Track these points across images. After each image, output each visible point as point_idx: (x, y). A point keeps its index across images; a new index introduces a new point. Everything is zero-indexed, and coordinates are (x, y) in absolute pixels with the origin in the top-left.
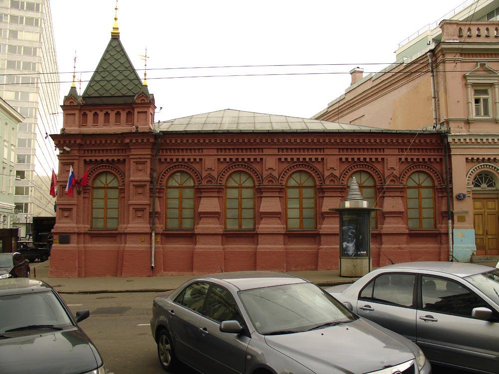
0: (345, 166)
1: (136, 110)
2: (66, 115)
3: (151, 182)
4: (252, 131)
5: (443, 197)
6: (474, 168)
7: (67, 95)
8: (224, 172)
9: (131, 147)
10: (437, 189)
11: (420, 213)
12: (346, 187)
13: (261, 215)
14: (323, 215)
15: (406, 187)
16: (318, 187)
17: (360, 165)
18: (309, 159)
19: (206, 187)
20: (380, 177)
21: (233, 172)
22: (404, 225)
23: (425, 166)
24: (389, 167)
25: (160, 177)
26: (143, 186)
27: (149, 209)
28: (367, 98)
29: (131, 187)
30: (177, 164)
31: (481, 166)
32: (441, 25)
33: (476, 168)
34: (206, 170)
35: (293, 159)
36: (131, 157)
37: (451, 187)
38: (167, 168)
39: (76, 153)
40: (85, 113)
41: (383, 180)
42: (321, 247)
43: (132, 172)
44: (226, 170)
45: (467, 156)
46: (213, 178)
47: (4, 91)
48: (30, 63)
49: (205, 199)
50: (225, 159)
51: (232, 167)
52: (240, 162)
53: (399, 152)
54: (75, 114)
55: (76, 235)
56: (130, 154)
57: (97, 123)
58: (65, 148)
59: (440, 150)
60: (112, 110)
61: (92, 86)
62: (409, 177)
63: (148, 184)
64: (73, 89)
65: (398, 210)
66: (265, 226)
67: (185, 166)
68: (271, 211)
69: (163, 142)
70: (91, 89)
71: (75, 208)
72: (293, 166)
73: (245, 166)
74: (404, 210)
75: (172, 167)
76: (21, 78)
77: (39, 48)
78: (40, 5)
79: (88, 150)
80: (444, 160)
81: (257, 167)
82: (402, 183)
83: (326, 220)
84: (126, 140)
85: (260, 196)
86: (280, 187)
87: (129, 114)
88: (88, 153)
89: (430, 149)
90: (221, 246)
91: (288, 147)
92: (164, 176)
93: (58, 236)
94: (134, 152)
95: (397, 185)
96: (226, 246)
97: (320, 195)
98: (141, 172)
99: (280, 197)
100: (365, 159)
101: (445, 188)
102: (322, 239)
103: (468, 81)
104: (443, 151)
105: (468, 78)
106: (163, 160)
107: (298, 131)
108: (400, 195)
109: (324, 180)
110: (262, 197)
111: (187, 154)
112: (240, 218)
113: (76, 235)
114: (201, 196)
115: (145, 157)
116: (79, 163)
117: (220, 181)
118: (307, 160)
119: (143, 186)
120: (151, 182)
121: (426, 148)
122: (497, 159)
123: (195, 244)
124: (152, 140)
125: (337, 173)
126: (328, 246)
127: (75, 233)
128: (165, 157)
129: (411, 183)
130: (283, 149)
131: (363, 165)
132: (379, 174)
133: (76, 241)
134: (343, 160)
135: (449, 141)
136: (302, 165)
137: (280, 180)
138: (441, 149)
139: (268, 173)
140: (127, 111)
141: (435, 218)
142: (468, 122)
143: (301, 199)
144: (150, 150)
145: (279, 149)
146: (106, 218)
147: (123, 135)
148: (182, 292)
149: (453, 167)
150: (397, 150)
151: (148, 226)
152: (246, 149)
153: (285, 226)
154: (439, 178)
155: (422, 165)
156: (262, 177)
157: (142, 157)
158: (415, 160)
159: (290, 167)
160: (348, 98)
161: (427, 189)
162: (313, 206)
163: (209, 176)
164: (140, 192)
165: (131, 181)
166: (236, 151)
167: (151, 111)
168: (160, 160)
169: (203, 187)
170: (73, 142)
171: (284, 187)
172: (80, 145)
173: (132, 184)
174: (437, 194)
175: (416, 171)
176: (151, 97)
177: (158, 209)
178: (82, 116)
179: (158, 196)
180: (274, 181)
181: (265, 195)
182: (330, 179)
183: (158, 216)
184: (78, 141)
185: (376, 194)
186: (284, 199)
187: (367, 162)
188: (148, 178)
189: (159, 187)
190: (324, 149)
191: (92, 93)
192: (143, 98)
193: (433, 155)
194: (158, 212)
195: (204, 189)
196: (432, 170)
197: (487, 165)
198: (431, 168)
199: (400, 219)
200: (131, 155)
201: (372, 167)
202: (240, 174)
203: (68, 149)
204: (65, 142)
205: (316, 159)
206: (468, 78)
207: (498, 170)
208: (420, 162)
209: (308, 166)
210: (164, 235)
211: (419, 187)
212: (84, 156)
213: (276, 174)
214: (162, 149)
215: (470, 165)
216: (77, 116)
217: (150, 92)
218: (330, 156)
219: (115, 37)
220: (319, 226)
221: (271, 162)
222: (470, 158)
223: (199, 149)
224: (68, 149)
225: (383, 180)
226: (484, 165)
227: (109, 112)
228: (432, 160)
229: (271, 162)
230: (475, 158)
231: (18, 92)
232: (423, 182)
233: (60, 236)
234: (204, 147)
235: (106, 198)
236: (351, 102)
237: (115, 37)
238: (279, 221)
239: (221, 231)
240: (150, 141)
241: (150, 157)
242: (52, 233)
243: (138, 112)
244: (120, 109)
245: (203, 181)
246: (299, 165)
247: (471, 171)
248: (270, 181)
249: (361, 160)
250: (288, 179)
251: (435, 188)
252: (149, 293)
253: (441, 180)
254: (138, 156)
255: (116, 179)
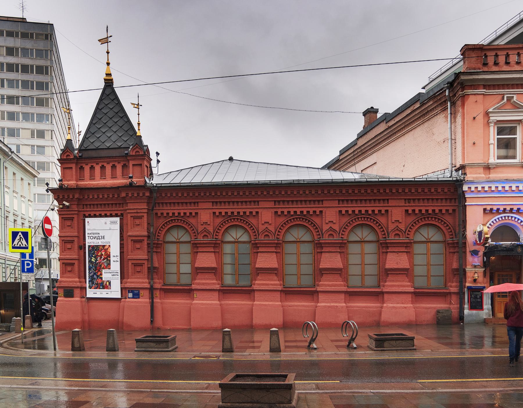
0: (345, 220)
1: (131, 163)
2: (64, 169)
3: (149, 237)
4: (401, 180)
5: (454, 252)
6: (490, 222)
7: (151, 162)
8: (220, 226)
9: (127, 202)
10: (448, 243)
11: (428, 271)
12: (346, 242)
13: (257, 271)
14: (321, 272)
15: (412, 241)
16: (316, 242)
17: (361, 218)
18: (281, 212)
19: (202, 242)
20: (383, 231)
21: (229, 227)
22: (409, 283)
23: (435, 218)
24: (394, 219)
25: (157, 232)
26: (141, 241)
27: (148, 264)
28: (406, 126)
29: (129, 240)
30: (173, 218)
31: (502, 217)
32: (462, 52)
33: (495, 220)
34: (263, 224)
35: (341, 211)
36: (128, 211)
37: (463, 241)
38: (163, 223)
39: (75, 208)
40: (82, 167)
41: (386, 234)
42: (319, 304)
43: (129, 228)
44: (222, 224)
45: (485, 207)
46: (209, 232)
47: (496, 252)
48: (28, 81)
49: (262, 254)
50: (220, 213)
51: (228, 221)
52: (236, 216)
53: (405, 203)
54: (72, 168)
55: (158, 291)
56: (127, 208)
57: (105, 177)
58: (64, 202)
59: (453, 201)
60: (107, 163)
61: (87, 138)
62: (417, 230)
63: (146, 239)
64: (69, 142)
65: (402, 267)
66: (260, 283)
67: (181, 220)
68: (268, 267)
69: (158, 195)
70: (509, 282)
71: (76, 219)
72: (290, 220)
73: (241, 220)
74: (409, 267)
75: (169, 221)
76: (35, 98)
77: (51, 83)
78: (49, 67)
79: (86, 205)
80: (457, 211)
81: (253, 221)
82: (407, 237)
83: (390, 277)
84: (122, 195)
85: (385, 251)
86: (276, 242)
87: (125, 167)
88: (87, 208)
89: (442, 199)
90: (218, 302)
91: (285, 199)
92: (346, 229)
93: (63, 290)
94: (130, 206)
95: (402, 239)
96: (223, 302)
97: (318, 251)
98: (138, 227)
99: (214, 252)
100: (367, 211)
101: (457, 243)
102: (320, 297)
103: (491, 118)
104: (457, 201)
105: (490, 115)
106: (159, 215)
107: (404, 180)
108: (406, 250)
109: (322, 234)
110: (258, 252)
111: (284, 206)
112: (299, 275)
113: (158, 291)
114: (322, 251)
115: (141, 211)
116: (78, 218)
117: (216, 235)
118: (305, 213)
119: (141, 241)
120: (149, 237)
121: (437, 197)
122: (521, 209)
123: (383, 302)
124: (148, 194)
125: (336, 227)
126: (326, 304)
127: (77, 287)
128: (161, 211)
129: (228, 238)
130: (279, 202)
131: (364, 218)
132: (382, 228)
133: (79, 295)
134: (409, 212)
135: (464, 190)
136: (300, 218)
137: (276, 235)
138: (455, 199)
139: (264, 227)
140: (111, 165)
141: (379, 275)
142: (488, 168)
143: (363, 254)
144: (146, 204)
145: (339, 200)
146: (179, 273)
147: (117, 189)
148: (366, 133)
149: (467, 219)
150: (403, 201)
151: (147, 280)
152: (242, 202)
153: (282, 282)
154: (451, 231)
155: (432, 218)
156: (258, 232)
157: (139, 211)
158: (423, 212)
159: (287, 221)
160: (360, 143)
161: (436, 244)
162: (311, 262)
163: (205, 230)
164: (138, 271)
165: (129, 236)
166: (231, 204)
167: (145, 163)
168: (156, 214)
169: (199, 242)
170: (71, 197)
171: (281, 242)
172: (79, 199)
173: (129, 215)
174: (447, 249)
175: (166, 232)
176: (145, 148)
177: (156, 265)
178: (78, 170)
179: (156, 251)
180: (269, 235)
181: (201, 251)
182: (136, 150)
183: (156, 271)
184: (77, 196)
185: (379, 250)
186: (344, 255)
187: (369, 215)
188: (146, 233)
189: (156, 242)
190: (322, 201)
191: (218, 300)
192: (137, 150)
193: (445, 206)
194: (156, 267)
195: (199, 244)
196: (443, 223)
197: (508, 217)
198: (442, 221)
199: (212, 276)
200: (128, 209)
201: (374, 220)
202: (362, 227)
203: (67, 204)
204: (64, 197)
205: (380, 211)
206: (490, 115)
207: (522, 222)
208: (430, 214)
209: (306, 220)
210: (163, 290)
211: (362, 242)
212: (83, 211)
213: (272, 228)
214: (159, 203)
215: (488, 217)
216: (74, 169)
217: (145, 143)
218: (329, 209)
219: (109, 83)
220: (382, 284)
221: (205, 216)
222: (489, 208)
223: (194, 203)
224: (67, 204)
225: (386, 234)
226: (505, 217)
227: (105, 164)
228: (444, 211)
229: (205, 216)
230: (495, 208)
231: (34, 146)
232: (431, 237)
233: (64, 290)
234: (199, 201)
235: (298, 254)
236: (363, 148)
237: (109, 83)
238: (276, 278)
239: (280, 288)
240: (146, 195)
241: (147, 211)
242: (344, 266)
243: (133, 165)
244: (115, 161)
245: (199, 236)
246: (297, 218)
247: (489, 223)
248: (205, 235)
249: (362, 213)
250: (349, 232)
251: (447, 242)
252: (163, 353)
253: (454, 234)
254: (135, 211)
255: (187, 233)
